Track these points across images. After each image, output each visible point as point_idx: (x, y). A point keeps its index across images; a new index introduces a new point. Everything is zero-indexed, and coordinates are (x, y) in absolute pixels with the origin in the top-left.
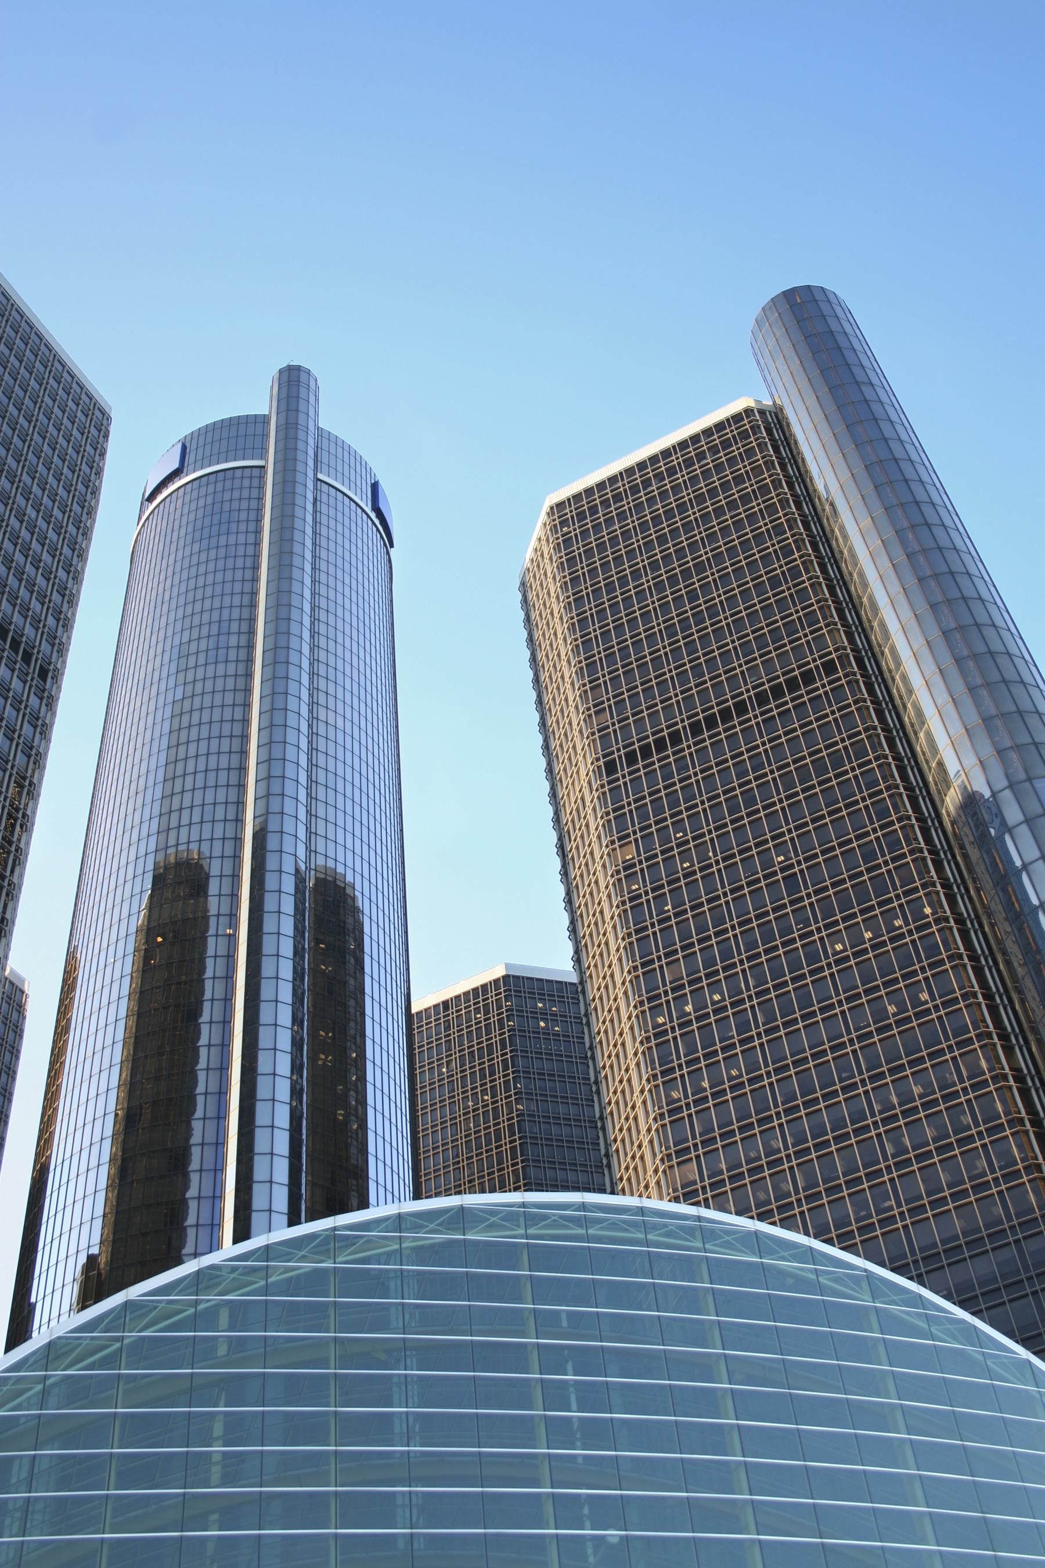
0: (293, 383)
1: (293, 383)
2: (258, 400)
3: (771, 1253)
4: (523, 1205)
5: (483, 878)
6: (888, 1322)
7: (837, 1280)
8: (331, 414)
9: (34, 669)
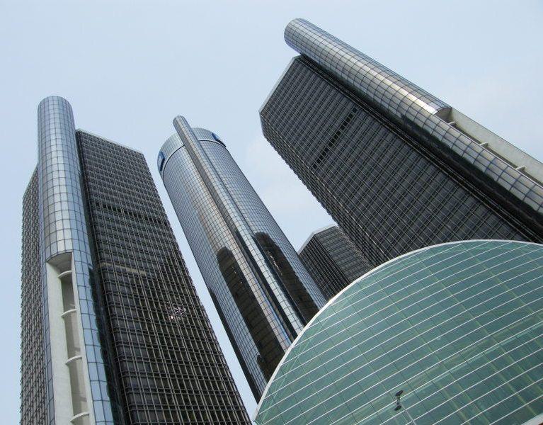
1: (179, 124)
3: (437, 252)
4: (371, 274)
5: (300, 215)
6: (474, 252)
7: (456, 248)
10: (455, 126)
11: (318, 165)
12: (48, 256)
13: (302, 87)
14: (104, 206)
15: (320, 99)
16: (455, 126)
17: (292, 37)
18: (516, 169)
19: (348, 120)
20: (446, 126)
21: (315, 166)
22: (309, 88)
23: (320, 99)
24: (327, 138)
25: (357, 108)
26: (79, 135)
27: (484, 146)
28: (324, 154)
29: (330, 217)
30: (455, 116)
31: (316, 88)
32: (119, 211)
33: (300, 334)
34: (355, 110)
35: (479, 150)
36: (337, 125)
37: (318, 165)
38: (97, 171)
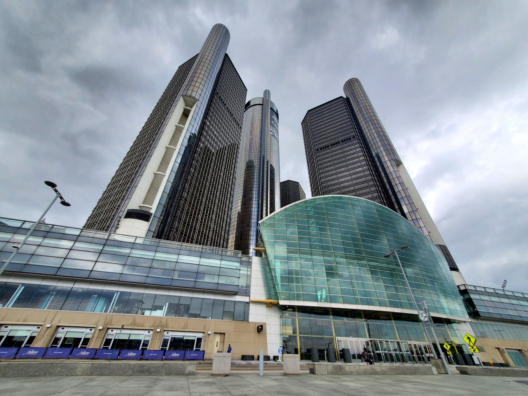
0: (267, 93)
1: (267, 93)
8: (272, 99)
12: (185, 94)
17: (352, 85)
21: (318, 150)
34: (354, 137)
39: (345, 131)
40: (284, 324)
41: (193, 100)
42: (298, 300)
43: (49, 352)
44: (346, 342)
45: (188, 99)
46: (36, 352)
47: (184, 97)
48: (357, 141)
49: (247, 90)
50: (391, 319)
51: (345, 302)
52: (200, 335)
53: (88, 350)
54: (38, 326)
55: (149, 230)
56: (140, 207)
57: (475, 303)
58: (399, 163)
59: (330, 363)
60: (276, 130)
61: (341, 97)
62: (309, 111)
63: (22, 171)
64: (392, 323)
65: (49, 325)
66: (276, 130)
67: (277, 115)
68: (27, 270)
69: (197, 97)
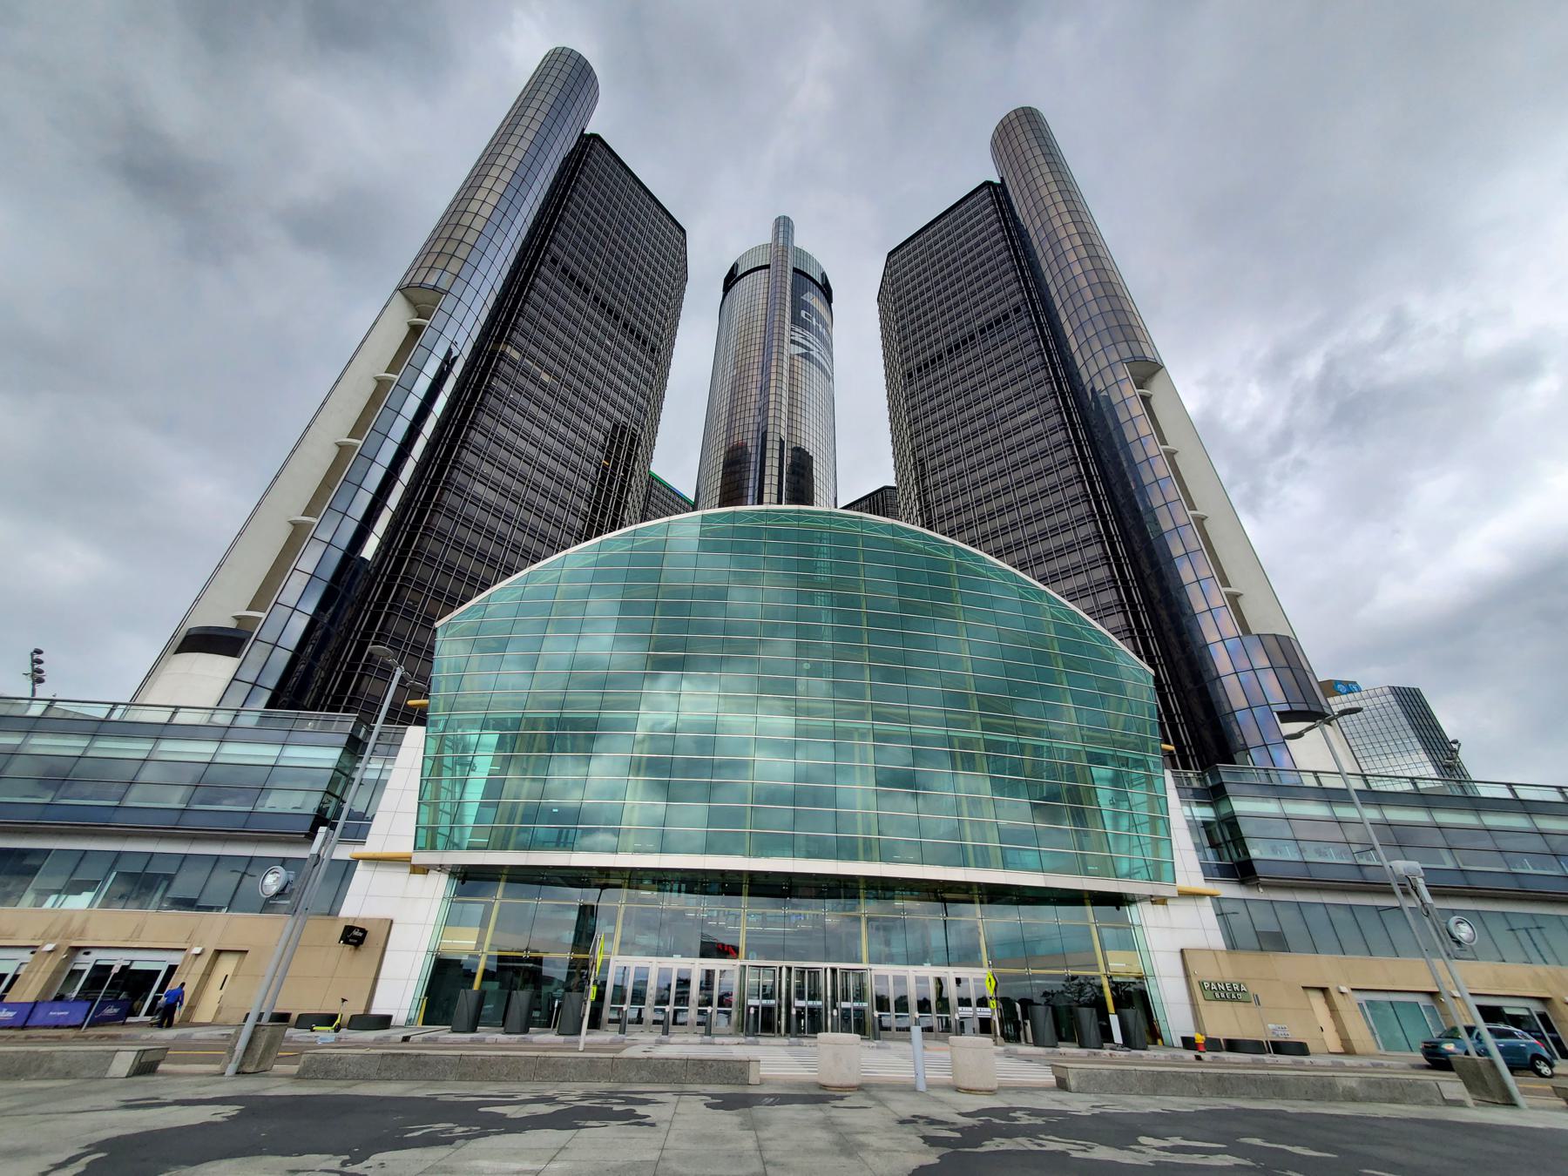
0: (784, 226)
1: (784, 226)
2: (767, 237)
8: (801, 240)
9: (648, 348)
10: (1146, 400)
11: (916, 374)
13: (981, 289)
14: (625, 326)
15: (1032, 469)
16: (1146, 400)
17: (1023, 134)
18: (1190, 513)
19: (998, 322)
20: (1129, 390)
21: (910, 375)
22: (991, 295)
23: (1032, 469)
24: (951, 338)
25: (1023, 309)
26: (590, 144)
27: (1196, 518)
28: (933, 362)
29: (893, 474)
30: (1156, 389)
31: (1019, 363)
32: (644, 343)
33: (769, 506)
35: (1182, 520)
36: (978, 323)
37: (916, 374)
38: (636, 289)
39: (1003, 301)
40: (451, 920)
41: (434, 295)
42: (868, 859)
43: (39, 1015)
44: (882, 979)
45: (416, 295)
46: (11, 1014)
47: (407, 291)
48: (1026, 321)
49: (683, 231)
50: (972, 902)
51: (709, 849)
52: (175, 958)
53: (11, 1006)
54: (33, 949)
55: (234, 679)
56: (237, 618)
57: (1246, 829)
58: (1147, 370)
59: (1041, 1050)
60: (819, 335)
61: (987, 184)
62: (891, 254)
63: (88, 565)
64: (1086, 918)
65: (197, 950)
66: (819, 335)
67: (826, 291)
68: (120, 819)
69: (443, 285)
